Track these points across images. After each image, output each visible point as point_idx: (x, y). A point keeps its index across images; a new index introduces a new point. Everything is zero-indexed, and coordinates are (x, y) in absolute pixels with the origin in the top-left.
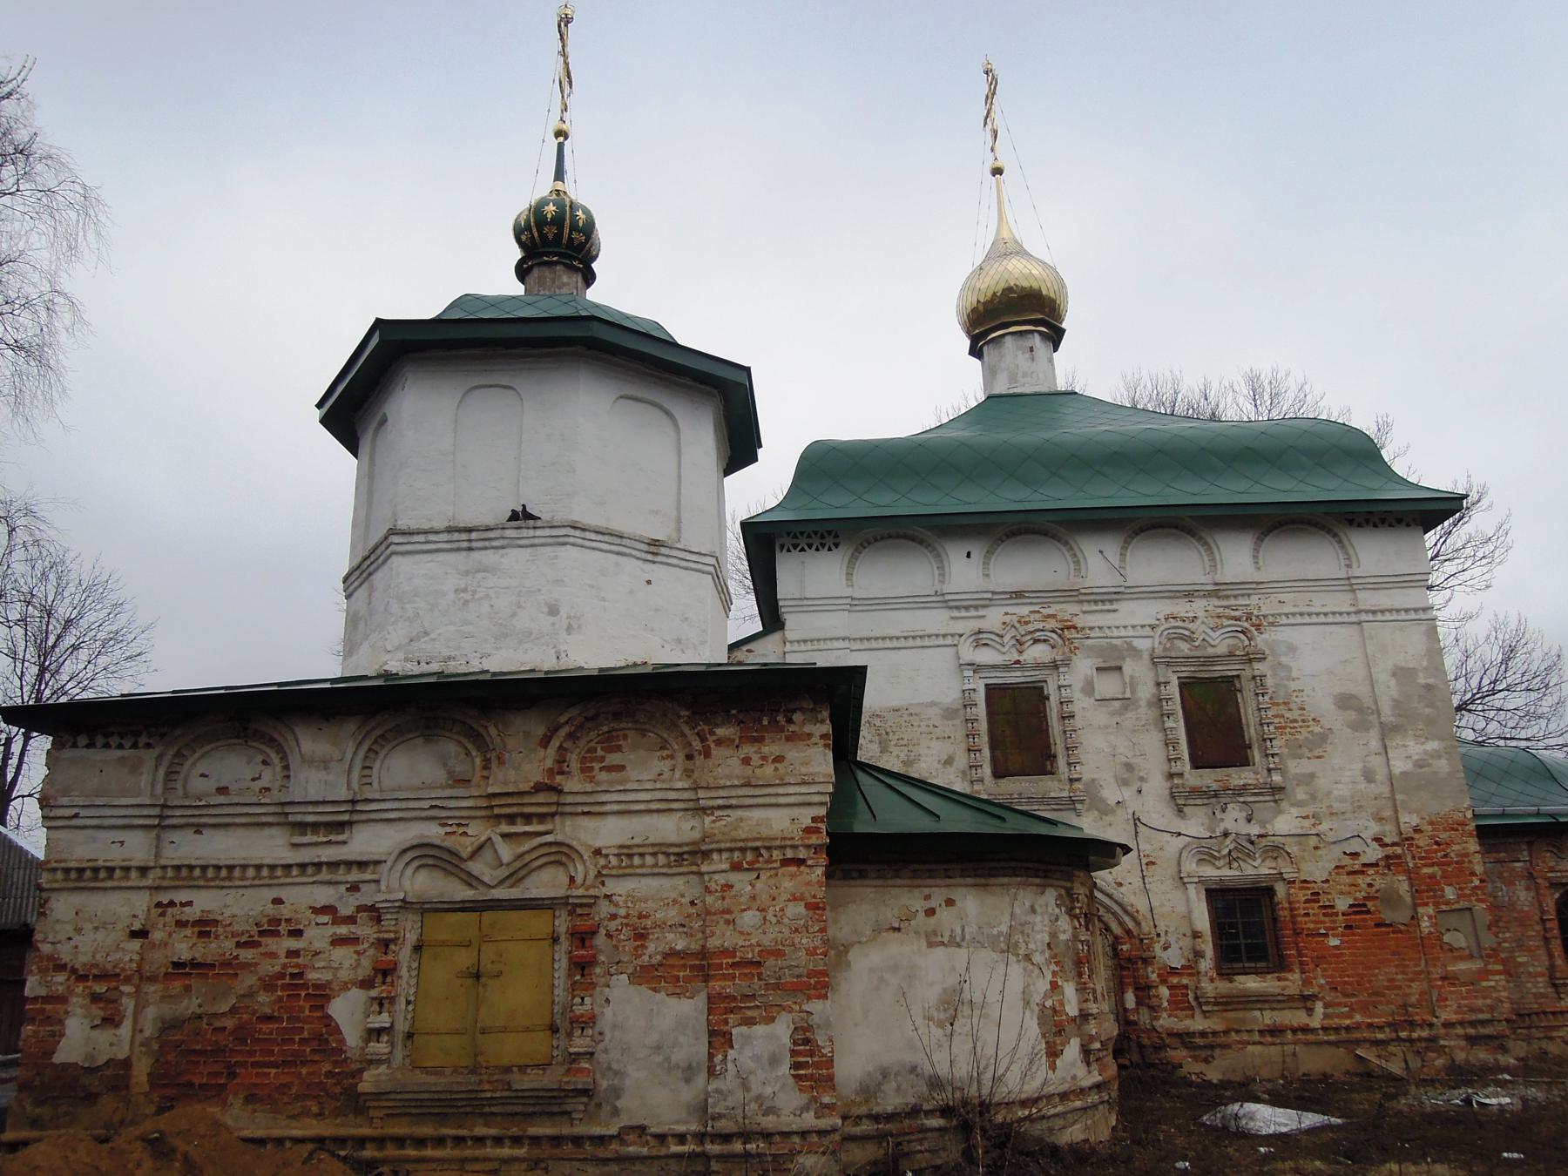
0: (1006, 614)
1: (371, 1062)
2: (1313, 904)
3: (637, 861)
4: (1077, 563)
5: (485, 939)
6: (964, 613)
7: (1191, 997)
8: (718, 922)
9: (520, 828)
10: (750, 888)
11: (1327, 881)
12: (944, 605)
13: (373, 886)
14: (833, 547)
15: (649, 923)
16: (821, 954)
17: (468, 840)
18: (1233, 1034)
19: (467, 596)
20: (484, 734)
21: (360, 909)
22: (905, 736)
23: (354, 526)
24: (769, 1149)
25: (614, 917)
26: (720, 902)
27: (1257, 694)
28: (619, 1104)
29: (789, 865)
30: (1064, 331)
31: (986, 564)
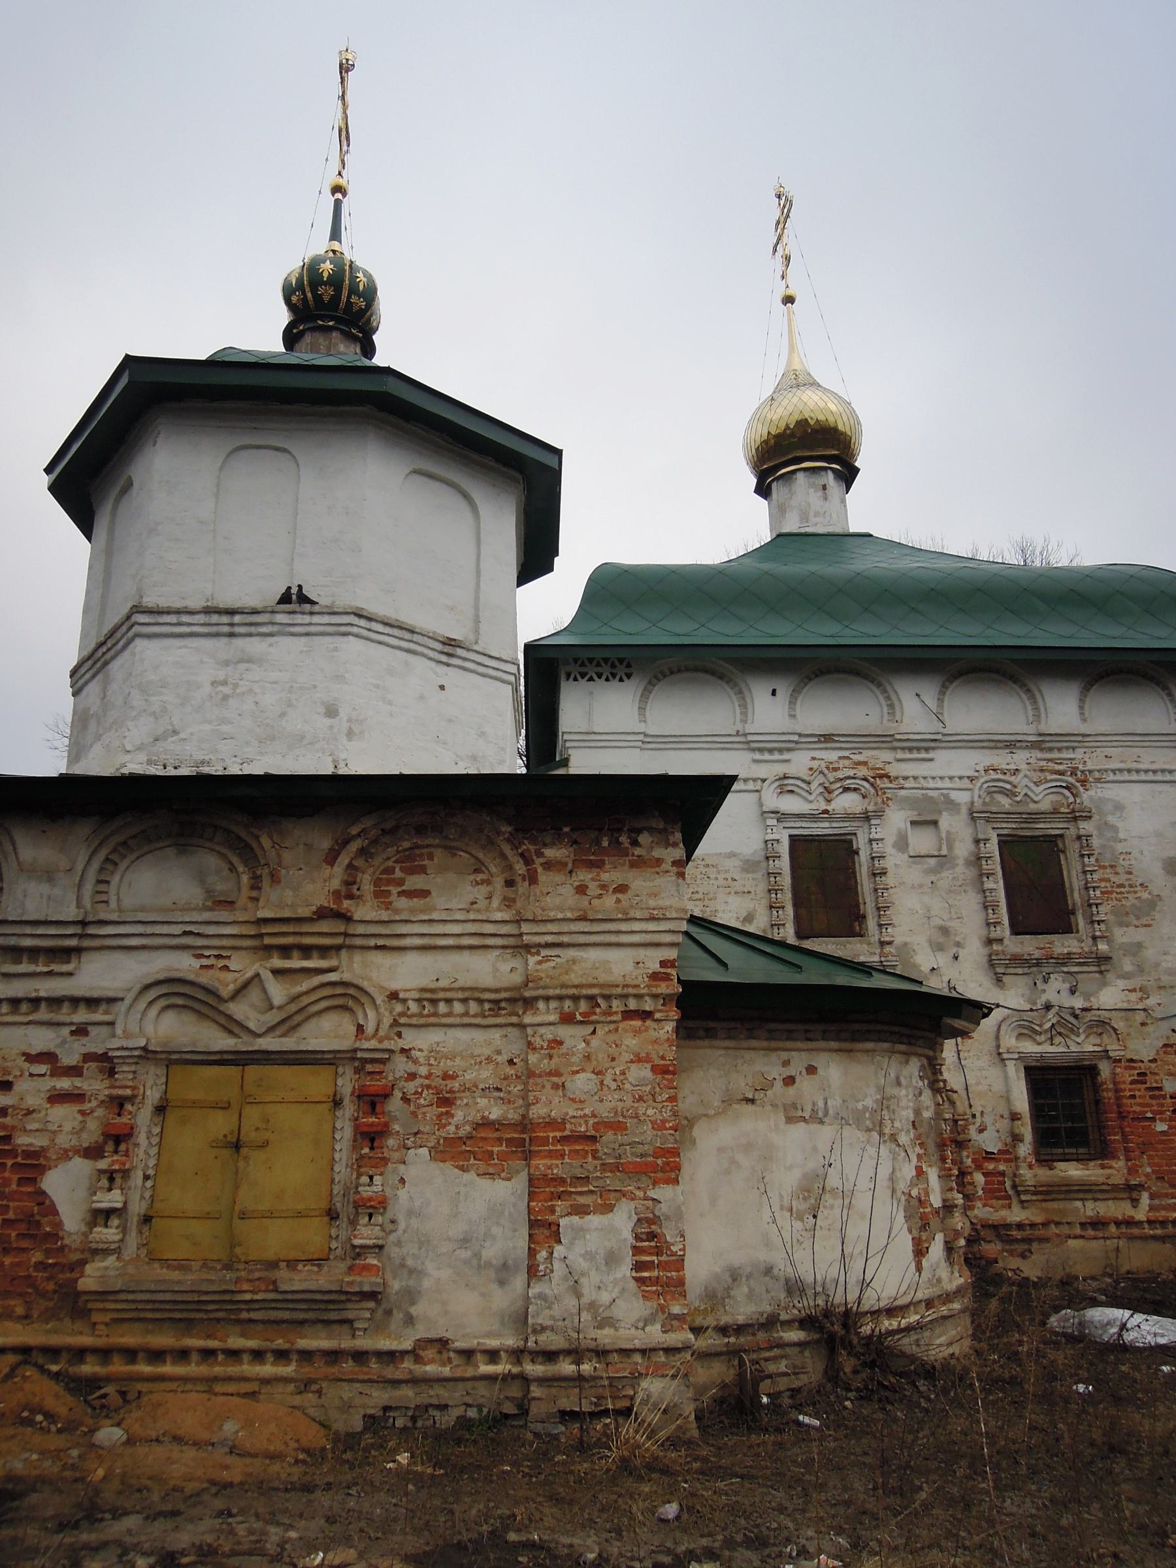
0: (813, 759)
1: (95, 1252)
2: (1139, 1086)
3: (442, 1008)
4: (891, 706)
5: (247, 1099)
6: (767, 756)
7: (1008, 1185)
8: (543, 1087)
9: (296, 963)
10: (584, 1045)
11: (1154, 1061)
12: (745, 746)
13: (104, 1030)
14: (625, 678)
15: (456, 1085)
16: (671, 1128)
17: (230, 976)
18: (1053, 1226)
19: (226, 690)
20: (254, 845)
21: (88, 1057)
22: (701, 890)
23: (85, 612)
24: (607, 1371)
25: (412, 1076)
26: (546, 1061)
27: (1082, 856)
28: (413, 1310)
29: (632, 1019)
30: (858, 470)
31: (792, 703)
